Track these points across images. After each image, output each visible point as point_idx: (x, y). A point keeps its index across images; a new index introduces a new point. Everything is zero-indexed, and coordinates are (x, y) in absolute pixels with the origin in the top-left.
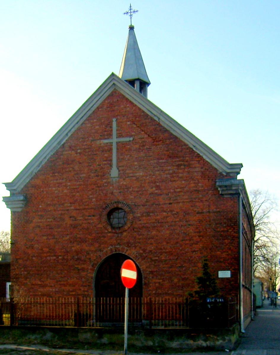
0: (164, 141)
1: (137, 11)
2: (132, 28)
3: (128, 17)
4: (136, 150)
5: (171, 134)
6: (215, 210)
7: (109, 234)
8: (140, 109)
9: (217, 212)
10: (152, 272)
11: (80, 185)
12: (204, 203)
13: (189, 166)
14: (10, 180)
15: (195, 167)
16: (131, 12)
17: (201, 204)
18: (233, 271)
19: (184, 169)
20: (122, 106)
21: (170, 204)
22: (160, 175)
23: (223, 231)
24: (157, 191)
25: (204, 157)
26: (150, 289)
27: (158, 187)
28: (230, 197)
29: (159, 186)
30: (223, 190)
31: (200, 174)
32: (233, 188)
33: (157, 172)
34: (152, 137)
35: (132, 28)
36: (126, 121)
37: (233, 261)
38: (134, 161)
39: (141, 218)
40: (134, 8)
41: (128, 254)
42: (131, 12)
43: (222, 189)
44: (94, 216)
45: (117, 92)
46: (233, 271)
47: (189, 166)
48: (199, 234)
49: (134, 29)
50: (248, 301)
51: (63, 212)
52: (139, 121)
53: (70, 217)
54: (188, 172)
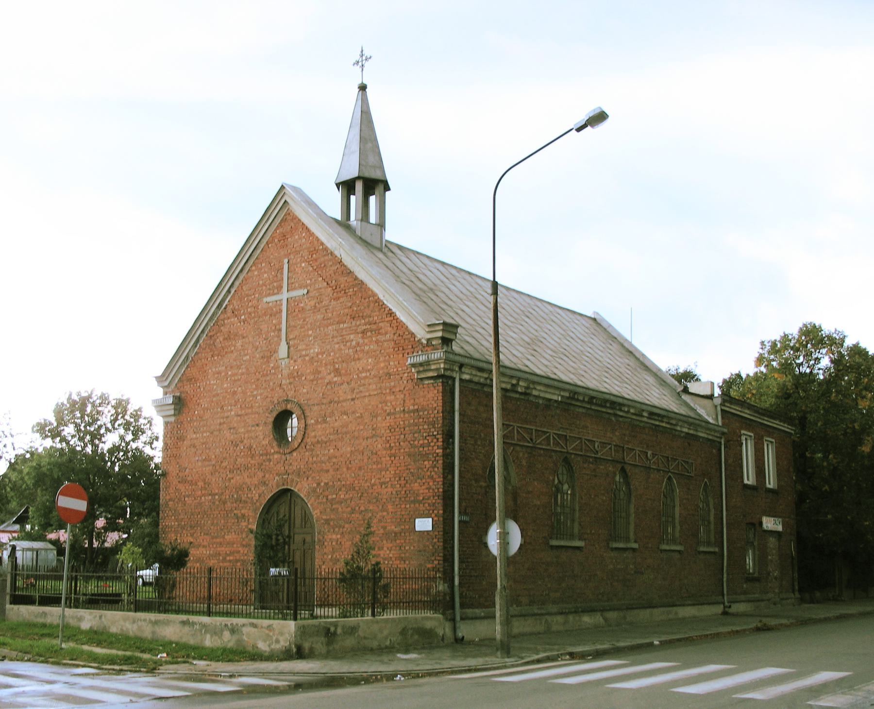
0: (347, 291)
1: (370, 57)
2: (363, 88)
3: (358, 68)
4: (310, 310)
5: (356, 278)
6: (411, 408)
7: (276, 456)
8: (318, 239)
9: (414, 411)
10: (327, 522)
11: (242, 374)
12: (398, 396)
13: (378, 331)
14: (160, 373)
15: (386, 333)
16: (362, 61)
17: (393, 397)
18: (435, 519)
19: (371, 337)
20: (297, 237)
21: (353, 399)
22: (340, 350)
23: (422, 446)
24: (335, 379)
25: (398, 314)
26: (325, 550)
27: (337, 372)
28: (433, 384)
29: (338, 369)
30: (418, 372)
31: (392, 344)
32: (433, 367)
33: (337, 346)
34: (331, 285)
35: (363, 88)
36: (301, 262)
37: (436, 500)
38: (308, 330)
39: (316, 427)
40: (367, 53)
41: (298, 490)
42: (362, 61)
43: (417, 370)
44: (257, 425)
45: (291, 214)
46: (435, 519)
47: (378, 331)
48: (389, 452)
49: (367, 90)
50: (753, 596)
51: (222, 421)
52: (316, 260)
53: (230, 429)
54: (377, 342)
